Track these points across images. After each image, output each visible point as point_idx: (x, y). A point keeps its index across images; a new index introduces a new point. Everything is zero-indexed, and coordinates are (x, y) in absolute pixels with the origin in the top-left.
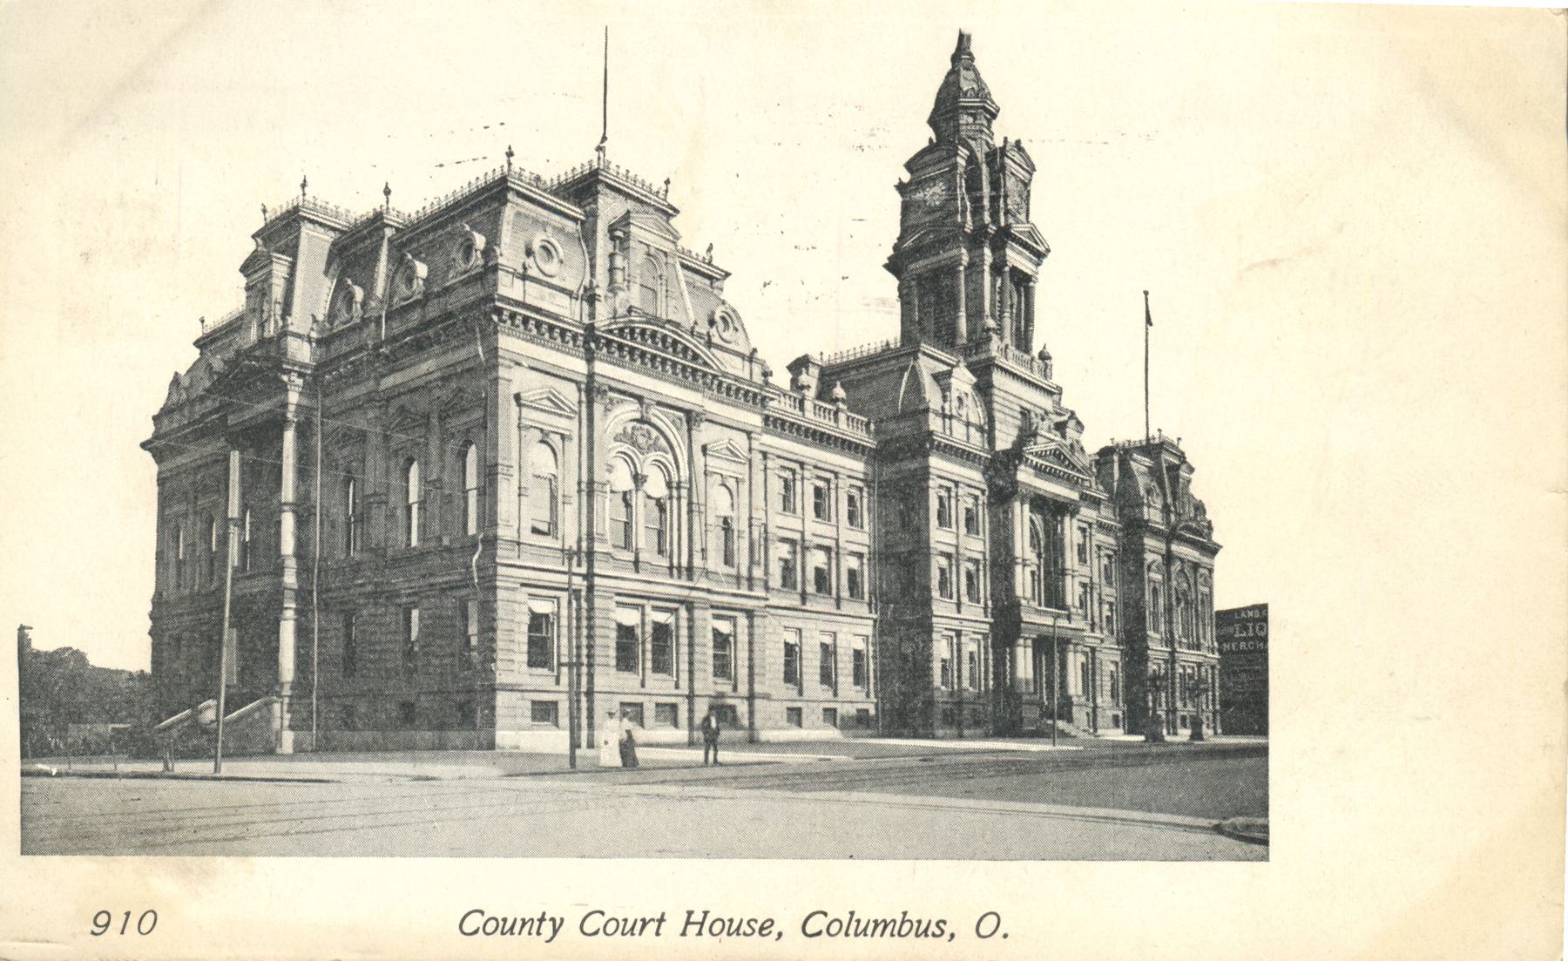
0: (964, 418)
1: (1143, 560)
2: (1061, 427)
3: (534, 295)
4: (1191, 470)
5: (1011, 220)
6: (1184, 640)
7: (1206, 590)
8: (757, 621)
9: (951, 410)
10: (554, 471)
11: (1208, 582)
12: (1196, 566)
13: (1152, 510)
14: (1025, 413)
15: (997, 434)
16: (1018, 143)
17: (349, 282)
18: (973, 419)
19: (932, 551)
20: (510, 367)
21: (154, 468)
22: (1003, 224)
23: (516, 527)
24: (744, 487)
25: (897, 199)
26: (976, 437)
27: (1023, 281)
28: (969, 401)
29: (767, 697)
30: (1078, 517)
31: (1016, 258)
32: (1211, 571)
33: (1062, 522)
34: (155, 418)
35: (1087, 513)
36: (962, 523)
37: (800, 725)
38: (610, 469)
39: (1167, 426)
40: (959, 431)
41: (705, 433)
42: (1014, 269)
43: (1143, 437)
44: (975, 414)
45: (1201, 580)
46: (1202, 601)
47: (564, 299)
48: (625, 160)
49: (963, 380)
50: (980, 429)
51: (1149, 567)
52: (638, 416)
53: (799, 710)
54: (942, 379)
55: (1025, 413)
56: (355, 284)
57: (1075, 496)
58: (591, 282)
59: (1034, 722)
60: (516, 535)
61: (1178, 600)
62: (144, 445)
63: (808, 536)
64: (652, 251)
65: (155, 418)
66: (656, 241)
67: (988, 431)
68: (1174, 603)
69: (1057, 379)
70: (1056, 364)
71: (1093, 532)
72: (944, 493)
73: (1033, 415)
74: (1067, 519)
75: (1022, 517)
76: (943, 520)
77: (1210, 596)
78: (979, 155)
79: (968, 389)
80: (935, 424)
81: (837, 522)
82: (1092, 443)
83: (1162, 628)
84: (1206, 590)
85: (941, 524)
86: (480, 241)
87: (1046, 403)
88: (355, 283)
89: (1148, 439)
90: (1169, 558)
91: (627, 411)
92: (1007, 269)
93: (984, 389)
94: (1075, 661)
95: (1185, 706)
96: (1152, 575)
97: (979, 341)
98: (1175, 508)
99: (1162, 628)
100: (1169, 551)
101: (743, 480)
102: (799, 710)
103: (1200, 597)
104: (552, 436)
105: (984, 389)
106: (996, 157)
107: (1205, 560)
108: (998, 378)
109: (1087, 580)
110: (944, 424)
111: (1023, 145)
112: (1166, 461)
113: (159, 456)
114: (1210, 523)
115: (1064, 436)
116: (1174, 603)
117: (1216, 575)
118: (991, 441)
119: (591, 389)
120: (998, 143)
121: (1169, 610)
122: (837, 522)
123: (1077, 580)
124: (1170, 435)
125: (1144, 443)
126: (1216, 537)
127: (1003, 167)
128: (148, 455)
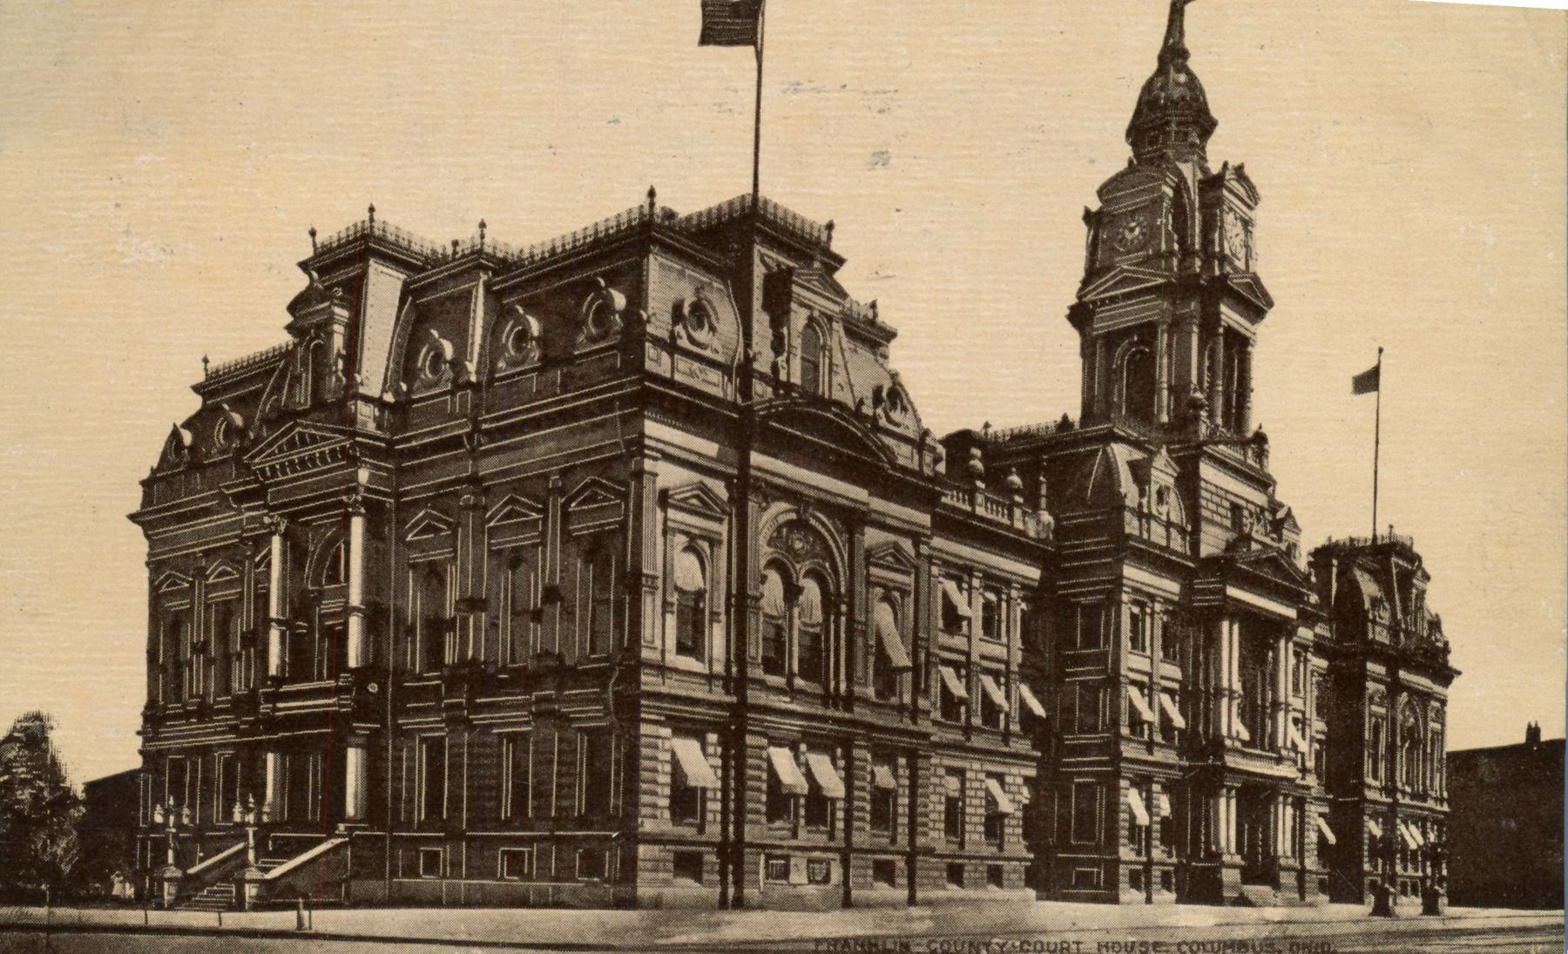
0: (1164, 518)
1: (1364, 688)
2: (1277, 526)
3: (685, 372)
4: (1427, 577)
5: (1228, 269)
6: (1408, 789)
7: (1438, 726)
8: (921, 763)
9: (1149, 507)
10: (702, 585)
11: (1440, 716)
12: (1425, 697)
13: (1378, 629)
14: (1236, 509)
15: (1203, 536)
16: (1239, 170)
17: (435, 333)
18: (1174, 518)
19: (1122, 679)
20: (655, 459)
21: (143, 546)
22: (1217, 272)
23: (660, 647)
24: (911, 600)
25: (1082, 233)
26: (1177, 543)
27: (1239, 344)
28: (1172, 497)
29: (930, 852)
30: (1295, 639)
31: (1229, 315)
32: (1443, 702)
33: (1276, 650)
34: (144, 483)
35: (1305, 633)
36: (1158, 643)
37: (999, 884)
38: (764, 579)
39: (1400, 522)
40: (1157, 534)
41: (872, 537)
42: (1229, 330)
43: (1370, 536)
44: (1173, 509)
45: (1431, 714)
46: (1432, 740)
47: (715, 376)
48: (783, 194)
49: (1163, 472)
50: (1182, 531)
51: (1371, 698)
52: (793, 516)
53: (961, 867)
54: (1140, 473)
55: (1236, 509)
56: (445, 338)
57: (1291, 613)
58: (746, 354)
59: (1234, 887)
60: (659, 658)
61: (1403, 740)
62: (133, 517)
63: (975, 657)
64: (816, 314)
65: (144, 483)
66: (823, 304)
67: (1193, 537)
68: (1399, 743)
69: (1273, 466)
70: (1272, 446)
71: (1309, 656)
72: (1136, 610)
73: (1246, 513)
74: (1282, 643)
75: (1230, 636)
76: (1137, 643)
77: (1440, 736)
78: (1190, 182)
79: (1170, 481)
80: (1131, 526)
81: (1009, 640)
82: (1308, 540)
83: (1382, 773)
84: (1438, 726)
85: (1134, 647)
86: (620, 300)
87: (1259, 498)
88: (443, 336)
89: (1375, 538)
90: (1395, 687)
91: (780, 510)
92: (1221, 330)
93: (1188, 484)
94: (1285, 816)
95: (1405, 869)
96: (1374, 708)
97: (1185, 417)
98: (1406, 623)
99: (1382, 773)
100: (1396, 679)
101: (909, 593)
102: (961, 867)
103: (1430, 735)
104: (700, 542)
105: (1188, 484)
106: (1212, 184)
107: (1437, 688)
108: (1207, 471)
109: (1299, 716)
110: (1141, 525)
111: (1247, 171)
112: (1397, 565)
113: (147, 527)
114: (1446, 644)
115: (1280, 540)
116: (1399, 743)
117: (1449, 709)
118: (1195, 546)
119: (744, 486)
120: (1214, 167)
121: (1392, 748)
122: (1009, 640)
123: (1291, 715)
124: (1402, 532)
125: (1369, 543)
126: (1454, 661)
127: (1220, 201)
128: (138, 529)
